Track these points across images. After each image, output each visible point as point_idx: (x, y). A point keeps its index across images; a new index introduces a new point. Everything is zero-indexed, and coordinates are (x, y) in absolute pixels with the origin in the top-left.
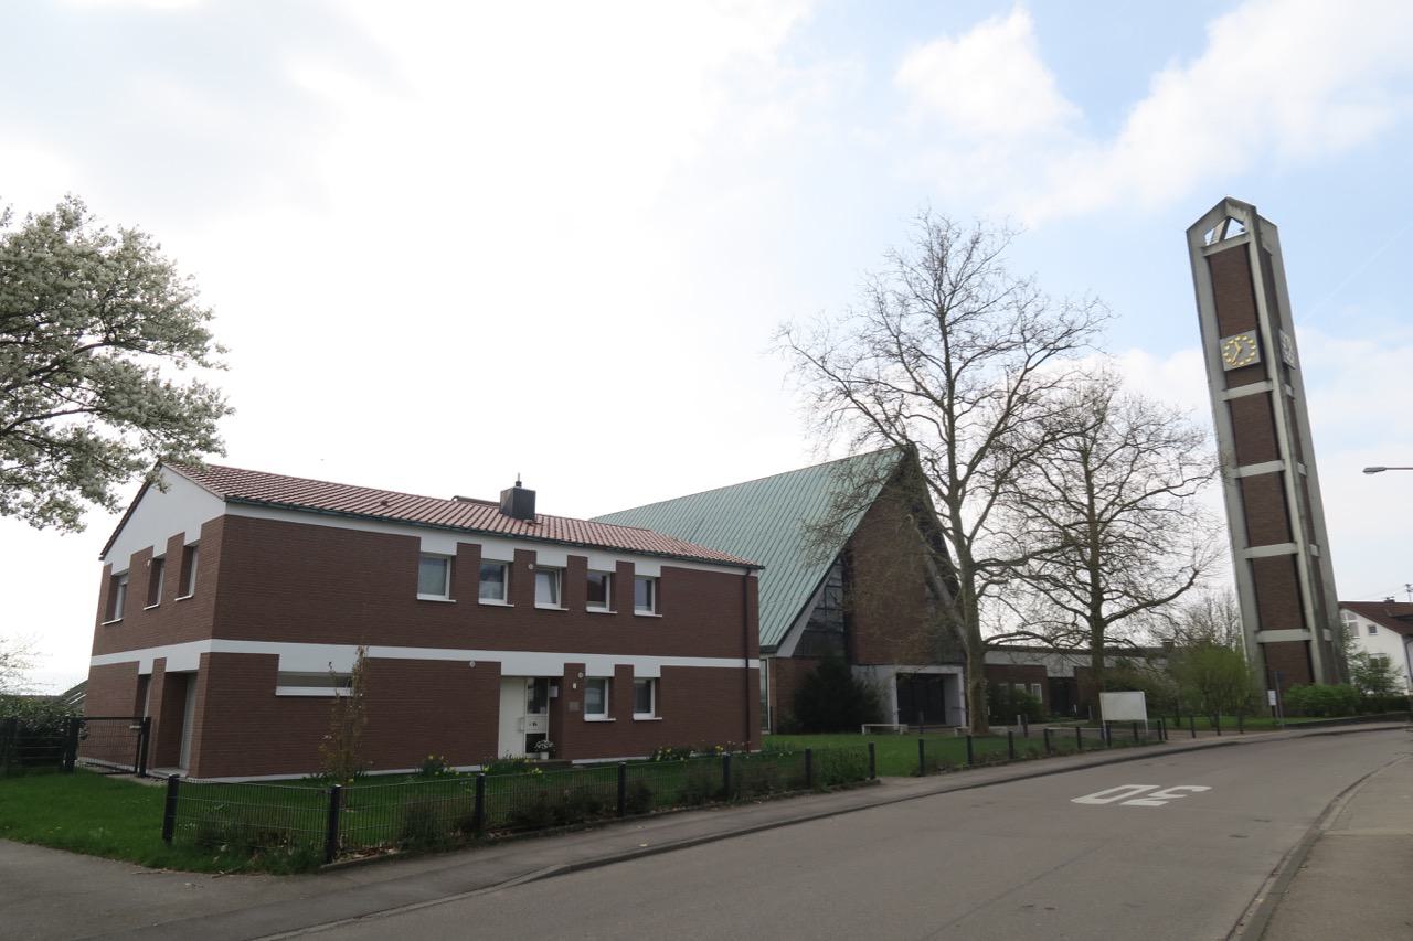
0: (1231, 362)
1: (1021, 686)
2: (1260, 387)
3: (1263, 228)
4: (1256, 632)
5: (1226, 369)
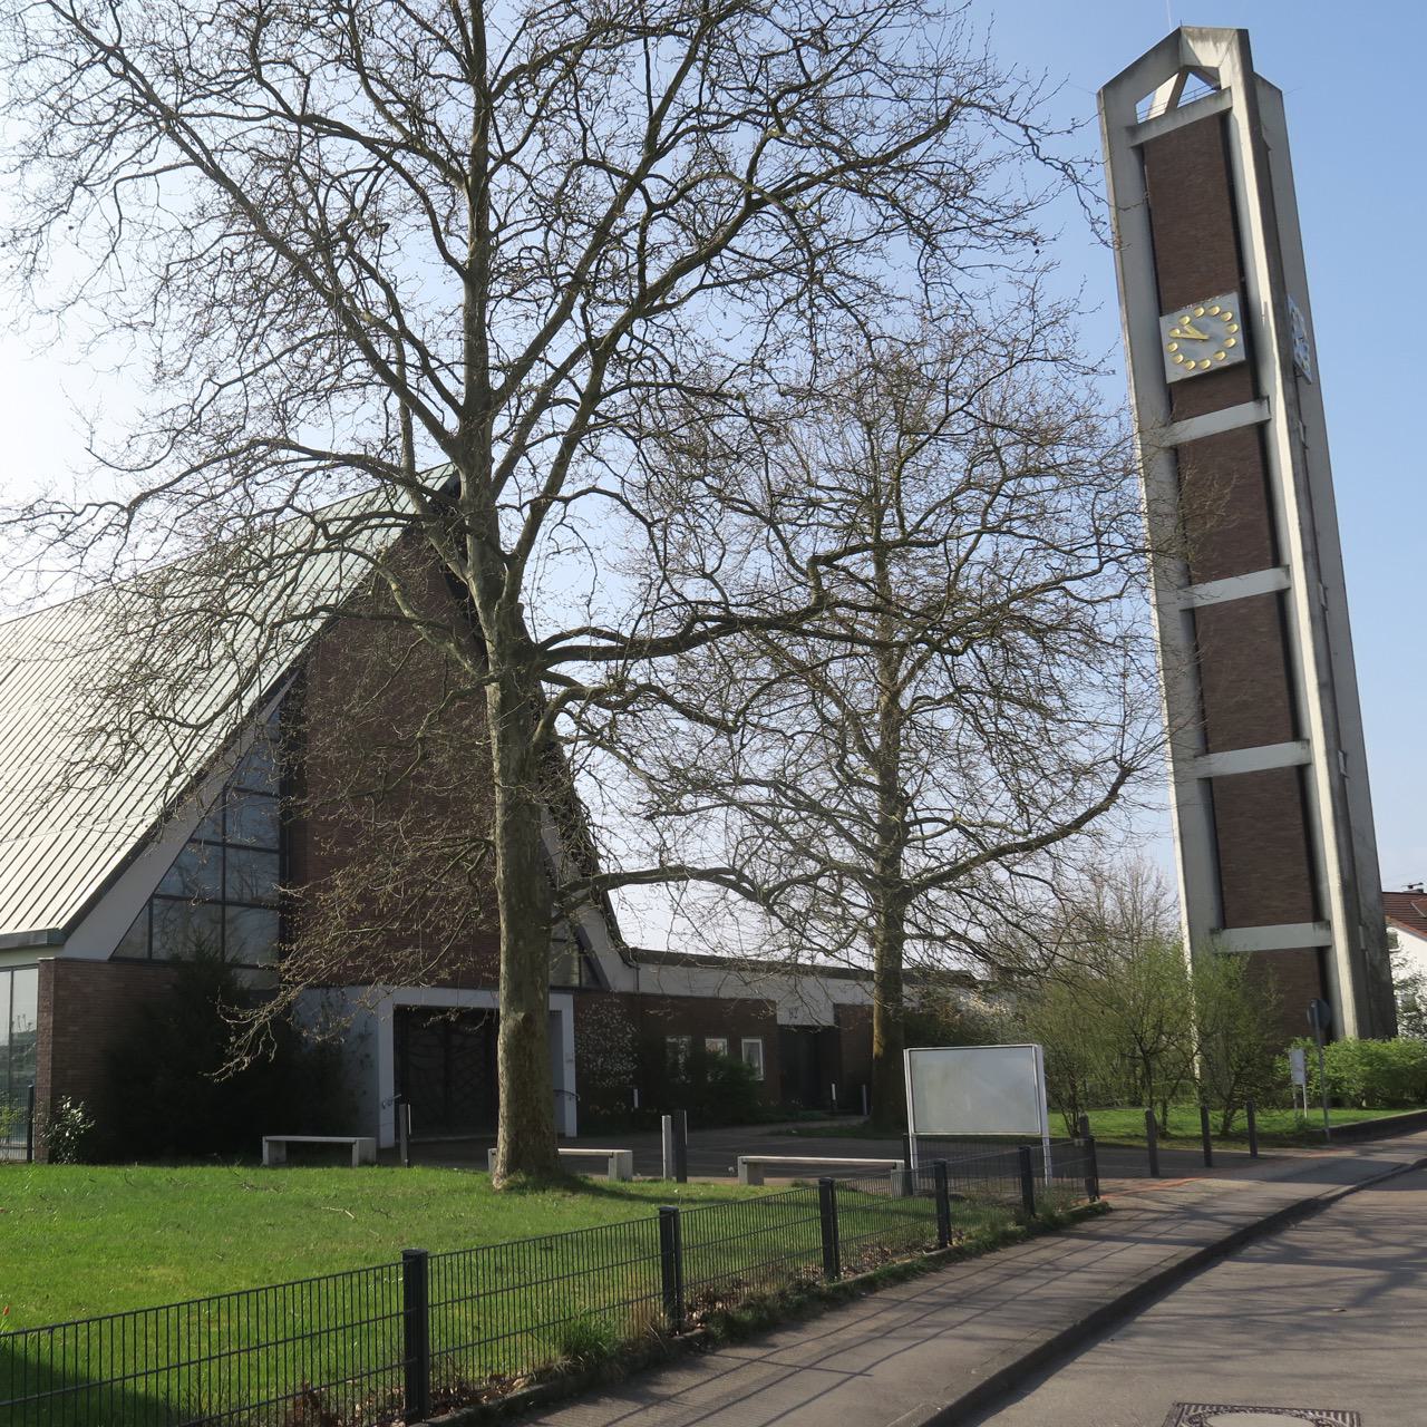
0: (1181, 366)
1: (718, 1045)
2: (1240, 415)
3: (1261, 93)
4: (1213, 932)
5: (1172, 377)
